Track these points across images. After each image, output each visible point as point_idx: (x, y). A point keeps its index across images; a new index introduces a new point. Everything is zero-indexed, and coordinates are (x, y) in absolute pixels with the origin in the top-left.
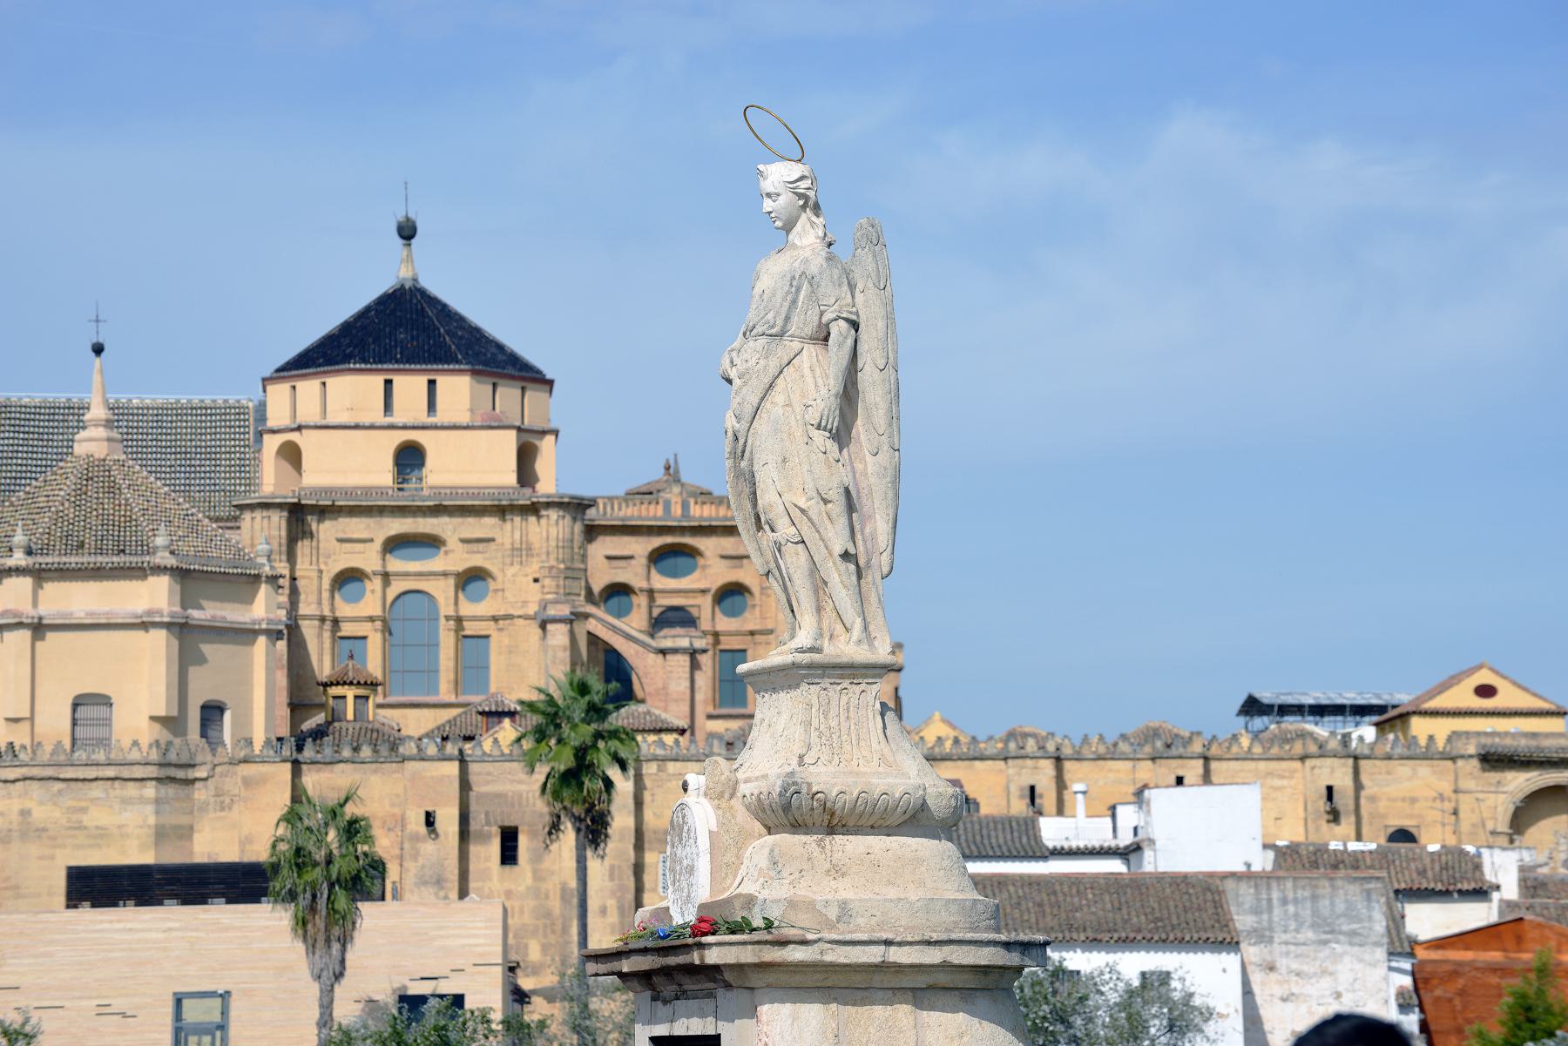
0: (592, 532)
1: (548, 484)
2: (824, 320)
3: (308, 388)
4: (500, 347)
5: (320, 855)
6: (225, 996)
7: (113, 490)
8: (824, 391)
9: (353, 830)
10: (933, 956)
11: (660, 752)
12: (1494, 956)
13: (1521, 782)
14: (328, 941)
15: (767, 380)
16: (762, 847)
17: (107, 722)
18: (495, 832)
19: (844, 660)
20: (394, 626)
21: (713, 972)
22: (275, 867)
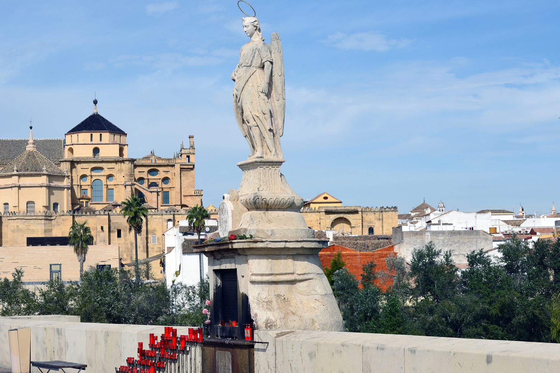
0: (135, 166)
1: (126, 156)
2: (263, 62)
3: (75, 136)
4: (115, 127)
5: (79, 235)
6: (60, 265)
7: (34, 157)
8: (263, 82)
9: (87, 230)
10: (299, 245)
11: (151, 213)
12: (329, 253)
13: (333, 217)
14: (82, 253)
15: (247, 79)
16: (247, 215)
17: (34, 207)
18: (116, 230)
19: (270, 160)
20: (93, 187)
21: (235, 251)
22: (70, 238)
